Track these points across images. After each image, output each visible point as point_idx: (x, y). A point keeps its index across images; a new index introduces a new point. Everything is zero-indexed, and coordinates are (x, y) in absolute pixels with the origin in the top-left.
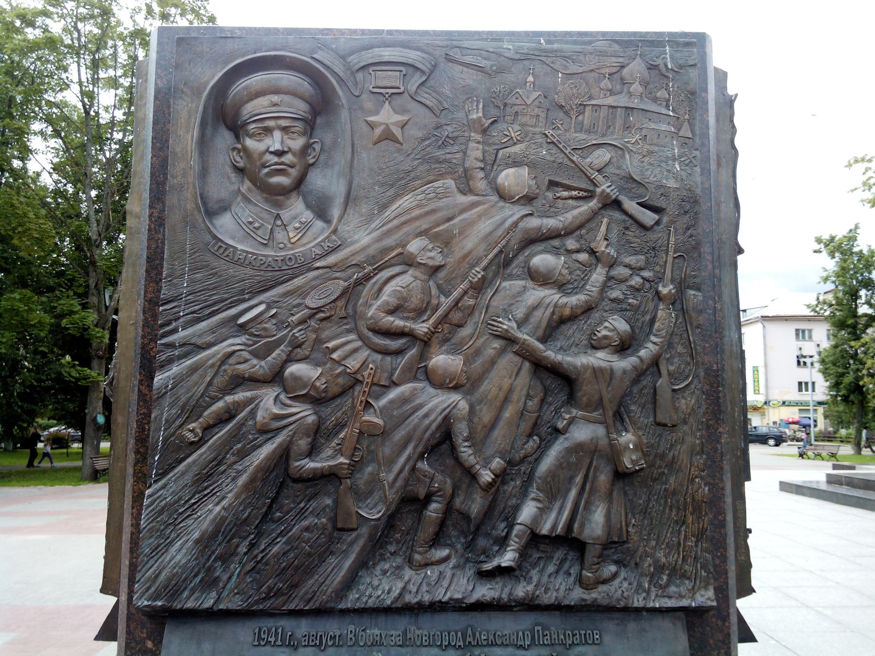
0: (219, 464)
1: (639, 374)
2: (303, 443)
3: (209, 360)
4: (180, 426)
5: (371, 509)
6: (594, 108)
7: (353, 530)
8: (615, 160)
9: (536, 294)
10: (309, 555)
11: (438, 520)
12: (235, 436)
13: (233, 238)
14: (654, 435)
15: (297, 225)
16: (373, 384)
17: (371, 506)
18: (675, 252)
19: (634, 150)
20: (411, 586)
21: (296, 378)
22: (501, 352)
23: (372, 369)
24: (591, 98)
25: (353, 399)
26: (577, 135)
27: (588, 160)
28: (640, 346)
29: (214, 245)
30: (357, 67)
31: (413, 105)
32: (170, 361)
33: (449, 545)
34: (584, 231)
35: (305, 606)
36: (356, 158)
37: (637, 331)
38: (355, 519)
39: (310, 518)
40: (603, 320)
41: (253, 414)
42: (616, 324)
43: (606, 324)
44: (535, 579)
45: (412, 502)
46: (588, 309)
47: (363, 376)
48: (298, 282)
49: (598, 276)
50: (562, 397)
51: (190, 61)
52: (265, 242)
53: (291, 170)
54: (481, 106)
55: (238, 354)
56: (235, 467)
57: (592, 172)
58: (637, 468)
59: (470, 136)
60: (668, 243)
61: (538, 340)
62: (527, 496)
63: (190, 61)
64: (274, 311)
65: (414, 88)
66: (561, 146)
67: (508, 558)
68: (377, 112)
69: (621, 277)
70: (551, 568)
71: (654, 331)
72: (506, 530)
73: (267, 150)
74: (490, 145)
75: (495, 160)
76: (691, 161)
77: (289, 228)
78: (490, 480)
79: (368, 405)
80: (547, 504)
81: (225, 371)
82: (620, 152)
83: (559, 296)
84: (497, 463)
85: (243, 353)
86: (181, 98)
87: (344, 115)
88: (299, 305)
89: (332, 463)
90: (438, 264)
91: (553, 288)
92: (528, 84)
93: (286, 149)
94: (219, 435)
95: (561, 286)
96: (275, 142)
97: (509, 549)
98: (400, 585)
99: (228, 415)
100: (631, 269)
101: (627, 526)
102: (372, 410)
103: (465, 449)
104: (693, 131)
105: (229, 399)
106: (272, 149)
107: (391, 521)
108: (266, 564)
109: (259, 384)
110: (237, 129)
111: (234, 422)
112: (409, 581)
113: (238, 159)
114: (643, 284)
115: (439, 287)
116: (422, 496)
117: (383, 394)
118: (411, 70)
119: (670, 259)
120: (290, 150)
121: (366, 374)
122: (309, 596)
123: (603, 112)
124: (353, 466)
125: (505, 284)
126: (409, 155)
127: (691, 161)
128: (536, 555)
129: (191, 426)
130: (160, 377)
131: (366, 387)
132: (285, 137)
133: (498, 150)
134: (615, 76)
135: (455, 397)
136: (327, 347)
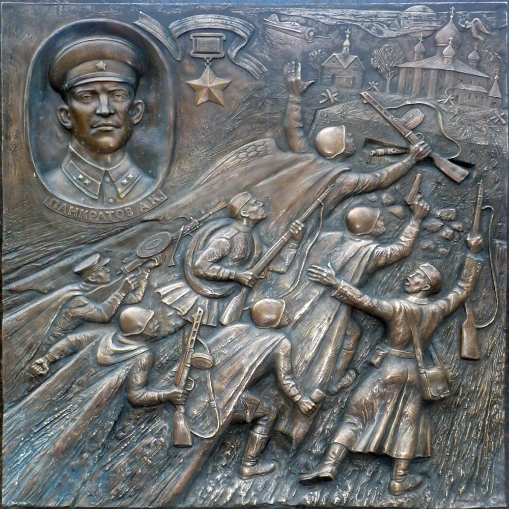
0: (67, 392)
1: (446, 317)
2: (139, 378)
3: (51, 303)
4: (29, 361)
5: (204, 430)
6: (409, 70)
7: (189, 447)
8: (428, 118)
9: (354, 245)
10: (150, 466)
11: (264, 440)
12: (80, 369)
13: (64, 193)
14: (458, 368)
15: (125, 181)
16: (201, 325)
17: (204, 428)
18: (483, 204)
19: (446, 110)
20: (242, 492)
21: (128, 320)
22: (322, 297)
23: (200, 312)
24: (406, 60)
25: (184, 338)
26: (393, 96)
27: (403, 119)
28: (447, 293)
29: (49, 200)
30: (177, 34)
31: (231, 69)
32: (17, 305)
33: (274, 460)
34: (398, 186)
35: (149, 505)
36: (179, 119)
37: (446, 277)
38: (189, 437)
39: (154, 435)
40: (415, 267)
41: (94, 350)
42: (427, 272)
43: (418, 271)
44: (350, 488)
45: (239, 426)
46: (402, 259)
47: (193, 319)
48: (127, 234)
49: (411, 228)
50: (378, 335)
51: (17, 27)
52: (96, 198)
53: (117, 131)
54: (299, 70)
55: (77, 299)
56: (81, 395)
57: (405, 130)
58: (442, 396)
59: (288, 98)
60: (477, 197)
61: (355, 286)
62: (343, 421)
63: (17, 27)
64: (108, 260)
65: (234, 54)
66: (376, 107)
67: (327, 470)
68: (198, 75)
69: (433, 228)
70: (364, 480)
71: (462, 277)
72: (324, 449)
73: (94, 112)
74: (308, 105)
75: (313, 121)
76: (499, 120)
77: (118, 183)
78: (310, 408)
79: (197, 343)
80: (361, 426)
81: (66, 313)
82: (433, 112)
83: (375, 245)
84: (317, 393)
85: (81, 298)
86: (10, 63)
87: (169, 81)
88: (131, 254)
89: (167, 392)
90: (260, 217)
91: (368, 239)
92: (345, 48)
93: (112, 111)
94: (64, 368)
95: (378, 238)
96: (103, 104)
97: (327, 463)
98: (231, 491)
99: (74, 349)
100: (442, 220)
101: (431, 444)
102: (201, 348)
103: (288, 382)
104: (502, 91)
105: (72, 337)
106: (98, 112)
107: (220, 442)
108: (115, 472)
109: (97, 325)
110: (66, 94)
111: (77, 356)
112: (239, 488)
113: (67, 120)
114: (453, 234)
115: (261, 239)
116: (249, 419)
117: (213, 335)
118: (230, 35)
119: (478, 212)
120: (116, 112)
121: (195, 316)
122: (153, 498)
123: (417, 75)
124: (187, 395)
125: (325, 235)
126: (230, 116)
127: (499, 120)
128: (351, 469)
129: (40, 360)
130: (7, 319)
131: (196, 327)
132: (111, 99)
133: (316, 111)
134: (429, 38)
135: (279, 336)
136: (159, 293)
